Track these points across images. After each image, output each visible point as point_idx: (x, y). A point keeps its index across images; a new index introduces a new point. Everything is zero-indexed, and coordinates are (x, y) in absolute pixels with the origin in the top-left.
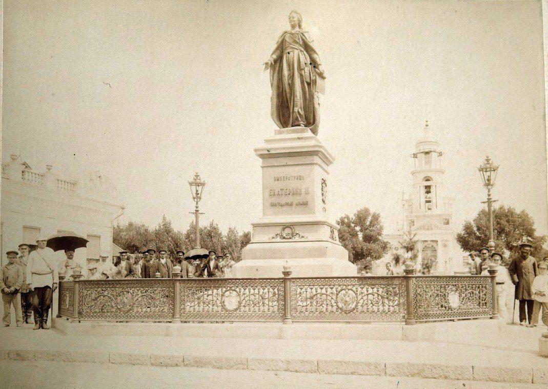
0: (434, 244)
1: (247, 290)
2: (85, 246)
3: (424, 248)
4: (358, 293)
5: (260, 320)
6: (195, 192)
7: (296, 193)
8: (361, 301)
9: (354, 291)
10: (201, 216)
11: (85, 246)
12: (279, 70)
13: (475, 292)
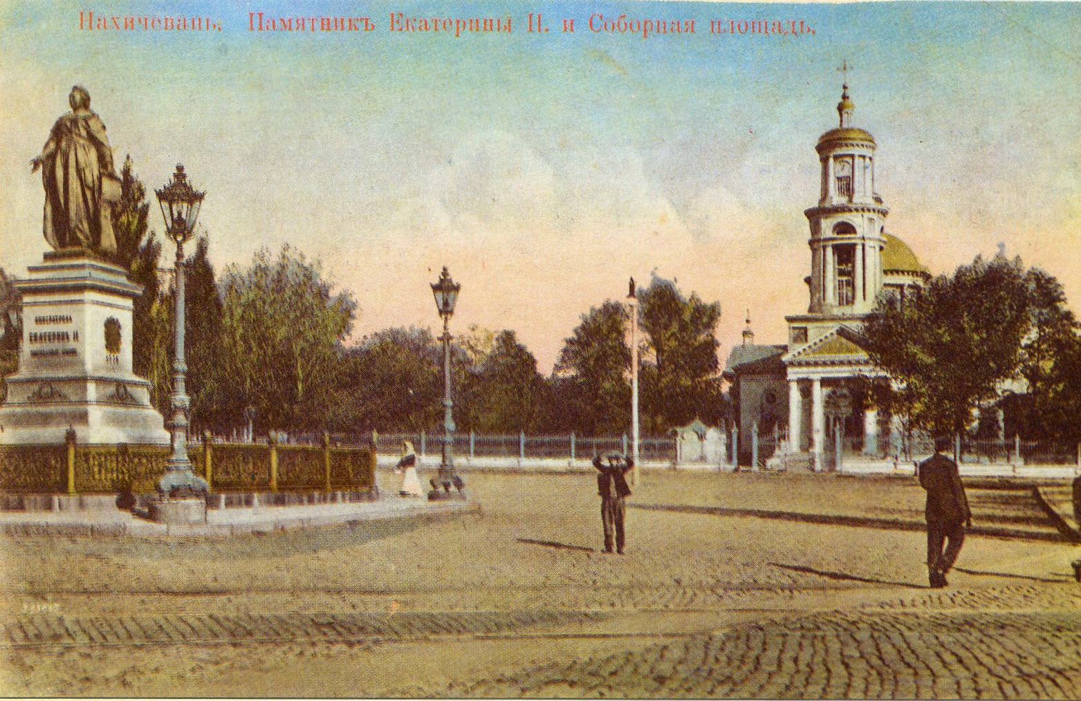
7: (62, 337)
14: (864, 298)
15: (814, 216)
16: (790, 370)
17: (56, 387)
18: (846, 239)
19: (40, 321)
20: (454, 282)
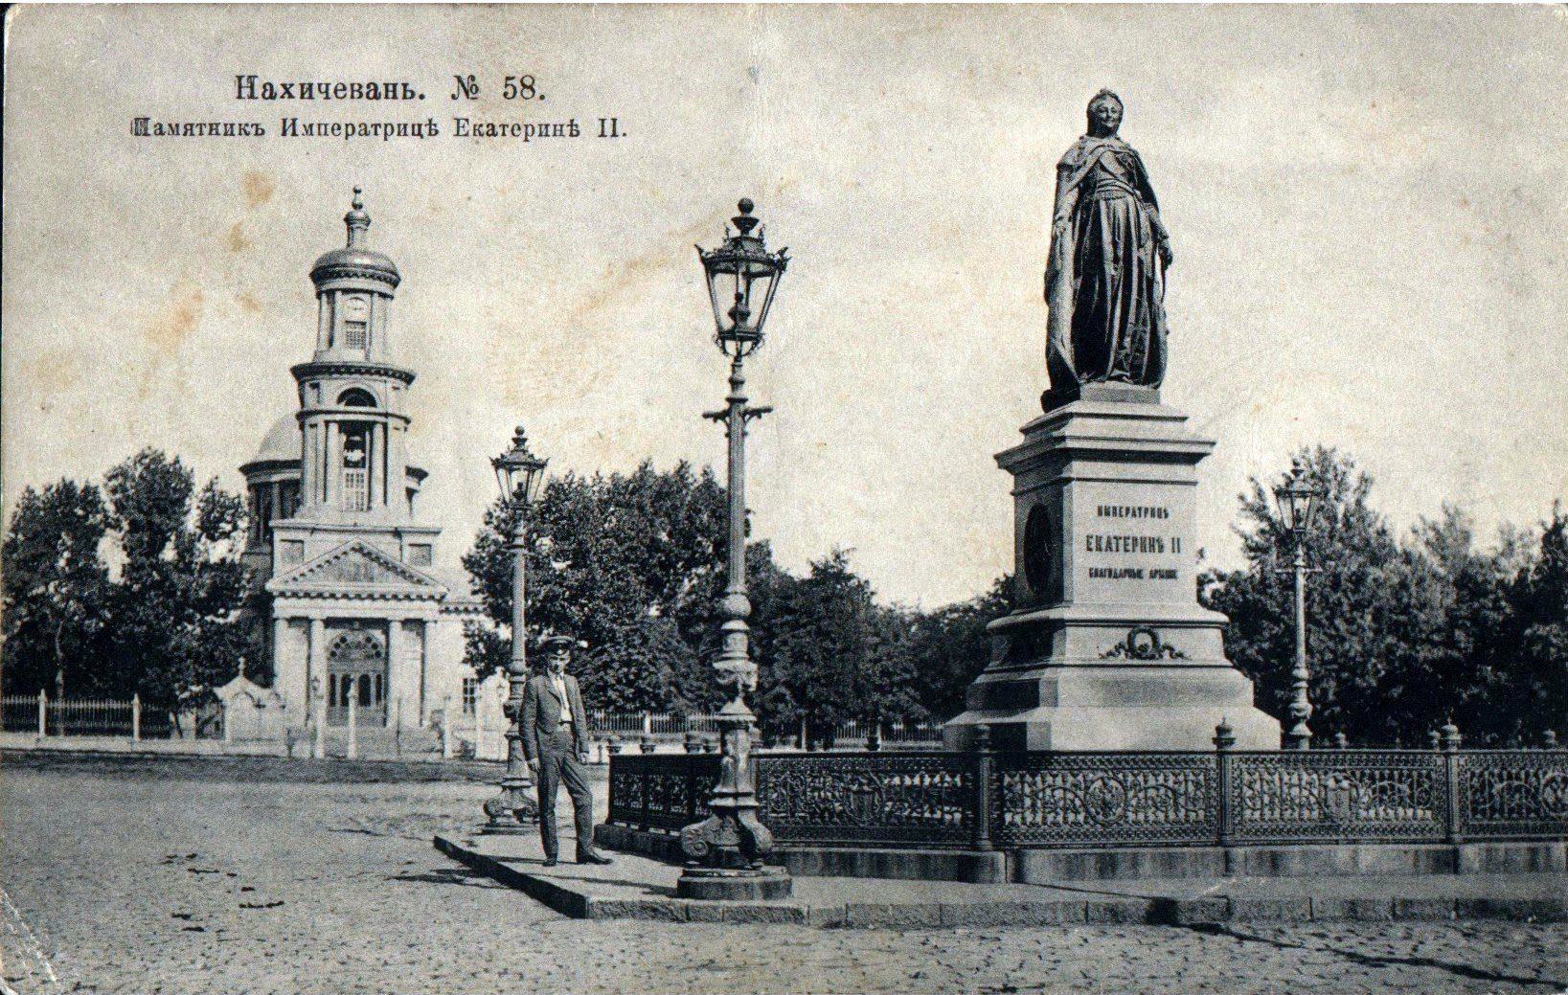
0: (378, 635)
1: (1038, 779)
2: (1004, 460)
3: (337, 646)
4: (1129, 784)
5: (1480, 836)
6: (731, 303)
7: (1153, 545)
8: (1134, 802)
9: (1120, 782)
10: (753, 425)
11: (1004, 460)
12: (1094, 221)
13: (1397, 785)
14: (385, 502)
15: (306, 374)
16: (279, 603)
17: (1166, 636)
18: (358, 414)
19: (1104, 512)
20: (1008, 480)
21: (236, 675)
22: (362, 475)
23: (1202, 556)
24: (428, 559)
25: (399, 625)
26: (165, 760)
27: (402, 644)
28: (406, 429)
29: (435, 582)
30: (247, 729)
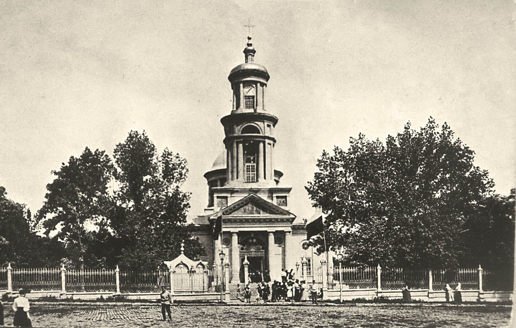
21: (180, 254)
22: (254, 166)
23: (174, 273)
24: (286, 204)
25: (275, 198)
26: (231, 273)
27: (274, 249)
28: (274, 145)
29: (289, 213)
30: (186, 286)
